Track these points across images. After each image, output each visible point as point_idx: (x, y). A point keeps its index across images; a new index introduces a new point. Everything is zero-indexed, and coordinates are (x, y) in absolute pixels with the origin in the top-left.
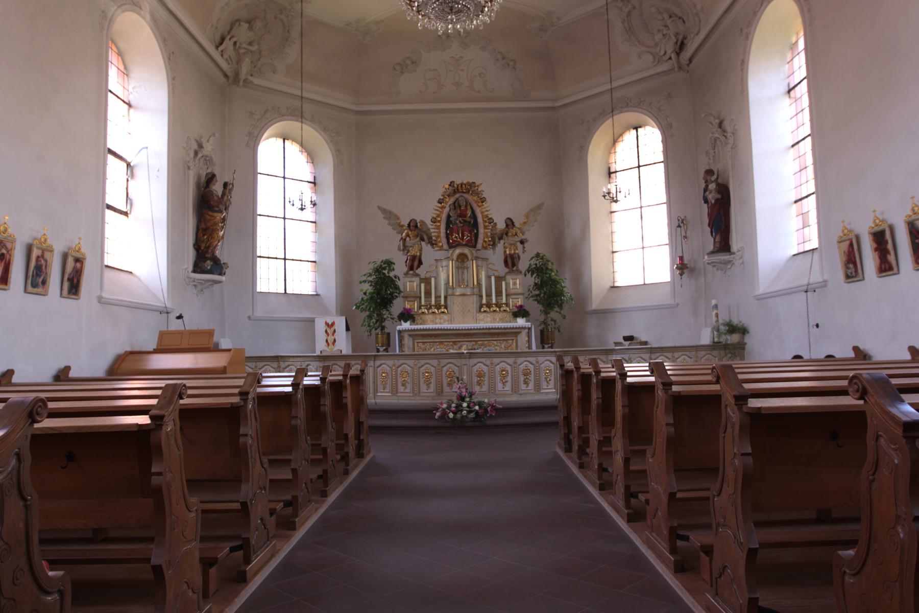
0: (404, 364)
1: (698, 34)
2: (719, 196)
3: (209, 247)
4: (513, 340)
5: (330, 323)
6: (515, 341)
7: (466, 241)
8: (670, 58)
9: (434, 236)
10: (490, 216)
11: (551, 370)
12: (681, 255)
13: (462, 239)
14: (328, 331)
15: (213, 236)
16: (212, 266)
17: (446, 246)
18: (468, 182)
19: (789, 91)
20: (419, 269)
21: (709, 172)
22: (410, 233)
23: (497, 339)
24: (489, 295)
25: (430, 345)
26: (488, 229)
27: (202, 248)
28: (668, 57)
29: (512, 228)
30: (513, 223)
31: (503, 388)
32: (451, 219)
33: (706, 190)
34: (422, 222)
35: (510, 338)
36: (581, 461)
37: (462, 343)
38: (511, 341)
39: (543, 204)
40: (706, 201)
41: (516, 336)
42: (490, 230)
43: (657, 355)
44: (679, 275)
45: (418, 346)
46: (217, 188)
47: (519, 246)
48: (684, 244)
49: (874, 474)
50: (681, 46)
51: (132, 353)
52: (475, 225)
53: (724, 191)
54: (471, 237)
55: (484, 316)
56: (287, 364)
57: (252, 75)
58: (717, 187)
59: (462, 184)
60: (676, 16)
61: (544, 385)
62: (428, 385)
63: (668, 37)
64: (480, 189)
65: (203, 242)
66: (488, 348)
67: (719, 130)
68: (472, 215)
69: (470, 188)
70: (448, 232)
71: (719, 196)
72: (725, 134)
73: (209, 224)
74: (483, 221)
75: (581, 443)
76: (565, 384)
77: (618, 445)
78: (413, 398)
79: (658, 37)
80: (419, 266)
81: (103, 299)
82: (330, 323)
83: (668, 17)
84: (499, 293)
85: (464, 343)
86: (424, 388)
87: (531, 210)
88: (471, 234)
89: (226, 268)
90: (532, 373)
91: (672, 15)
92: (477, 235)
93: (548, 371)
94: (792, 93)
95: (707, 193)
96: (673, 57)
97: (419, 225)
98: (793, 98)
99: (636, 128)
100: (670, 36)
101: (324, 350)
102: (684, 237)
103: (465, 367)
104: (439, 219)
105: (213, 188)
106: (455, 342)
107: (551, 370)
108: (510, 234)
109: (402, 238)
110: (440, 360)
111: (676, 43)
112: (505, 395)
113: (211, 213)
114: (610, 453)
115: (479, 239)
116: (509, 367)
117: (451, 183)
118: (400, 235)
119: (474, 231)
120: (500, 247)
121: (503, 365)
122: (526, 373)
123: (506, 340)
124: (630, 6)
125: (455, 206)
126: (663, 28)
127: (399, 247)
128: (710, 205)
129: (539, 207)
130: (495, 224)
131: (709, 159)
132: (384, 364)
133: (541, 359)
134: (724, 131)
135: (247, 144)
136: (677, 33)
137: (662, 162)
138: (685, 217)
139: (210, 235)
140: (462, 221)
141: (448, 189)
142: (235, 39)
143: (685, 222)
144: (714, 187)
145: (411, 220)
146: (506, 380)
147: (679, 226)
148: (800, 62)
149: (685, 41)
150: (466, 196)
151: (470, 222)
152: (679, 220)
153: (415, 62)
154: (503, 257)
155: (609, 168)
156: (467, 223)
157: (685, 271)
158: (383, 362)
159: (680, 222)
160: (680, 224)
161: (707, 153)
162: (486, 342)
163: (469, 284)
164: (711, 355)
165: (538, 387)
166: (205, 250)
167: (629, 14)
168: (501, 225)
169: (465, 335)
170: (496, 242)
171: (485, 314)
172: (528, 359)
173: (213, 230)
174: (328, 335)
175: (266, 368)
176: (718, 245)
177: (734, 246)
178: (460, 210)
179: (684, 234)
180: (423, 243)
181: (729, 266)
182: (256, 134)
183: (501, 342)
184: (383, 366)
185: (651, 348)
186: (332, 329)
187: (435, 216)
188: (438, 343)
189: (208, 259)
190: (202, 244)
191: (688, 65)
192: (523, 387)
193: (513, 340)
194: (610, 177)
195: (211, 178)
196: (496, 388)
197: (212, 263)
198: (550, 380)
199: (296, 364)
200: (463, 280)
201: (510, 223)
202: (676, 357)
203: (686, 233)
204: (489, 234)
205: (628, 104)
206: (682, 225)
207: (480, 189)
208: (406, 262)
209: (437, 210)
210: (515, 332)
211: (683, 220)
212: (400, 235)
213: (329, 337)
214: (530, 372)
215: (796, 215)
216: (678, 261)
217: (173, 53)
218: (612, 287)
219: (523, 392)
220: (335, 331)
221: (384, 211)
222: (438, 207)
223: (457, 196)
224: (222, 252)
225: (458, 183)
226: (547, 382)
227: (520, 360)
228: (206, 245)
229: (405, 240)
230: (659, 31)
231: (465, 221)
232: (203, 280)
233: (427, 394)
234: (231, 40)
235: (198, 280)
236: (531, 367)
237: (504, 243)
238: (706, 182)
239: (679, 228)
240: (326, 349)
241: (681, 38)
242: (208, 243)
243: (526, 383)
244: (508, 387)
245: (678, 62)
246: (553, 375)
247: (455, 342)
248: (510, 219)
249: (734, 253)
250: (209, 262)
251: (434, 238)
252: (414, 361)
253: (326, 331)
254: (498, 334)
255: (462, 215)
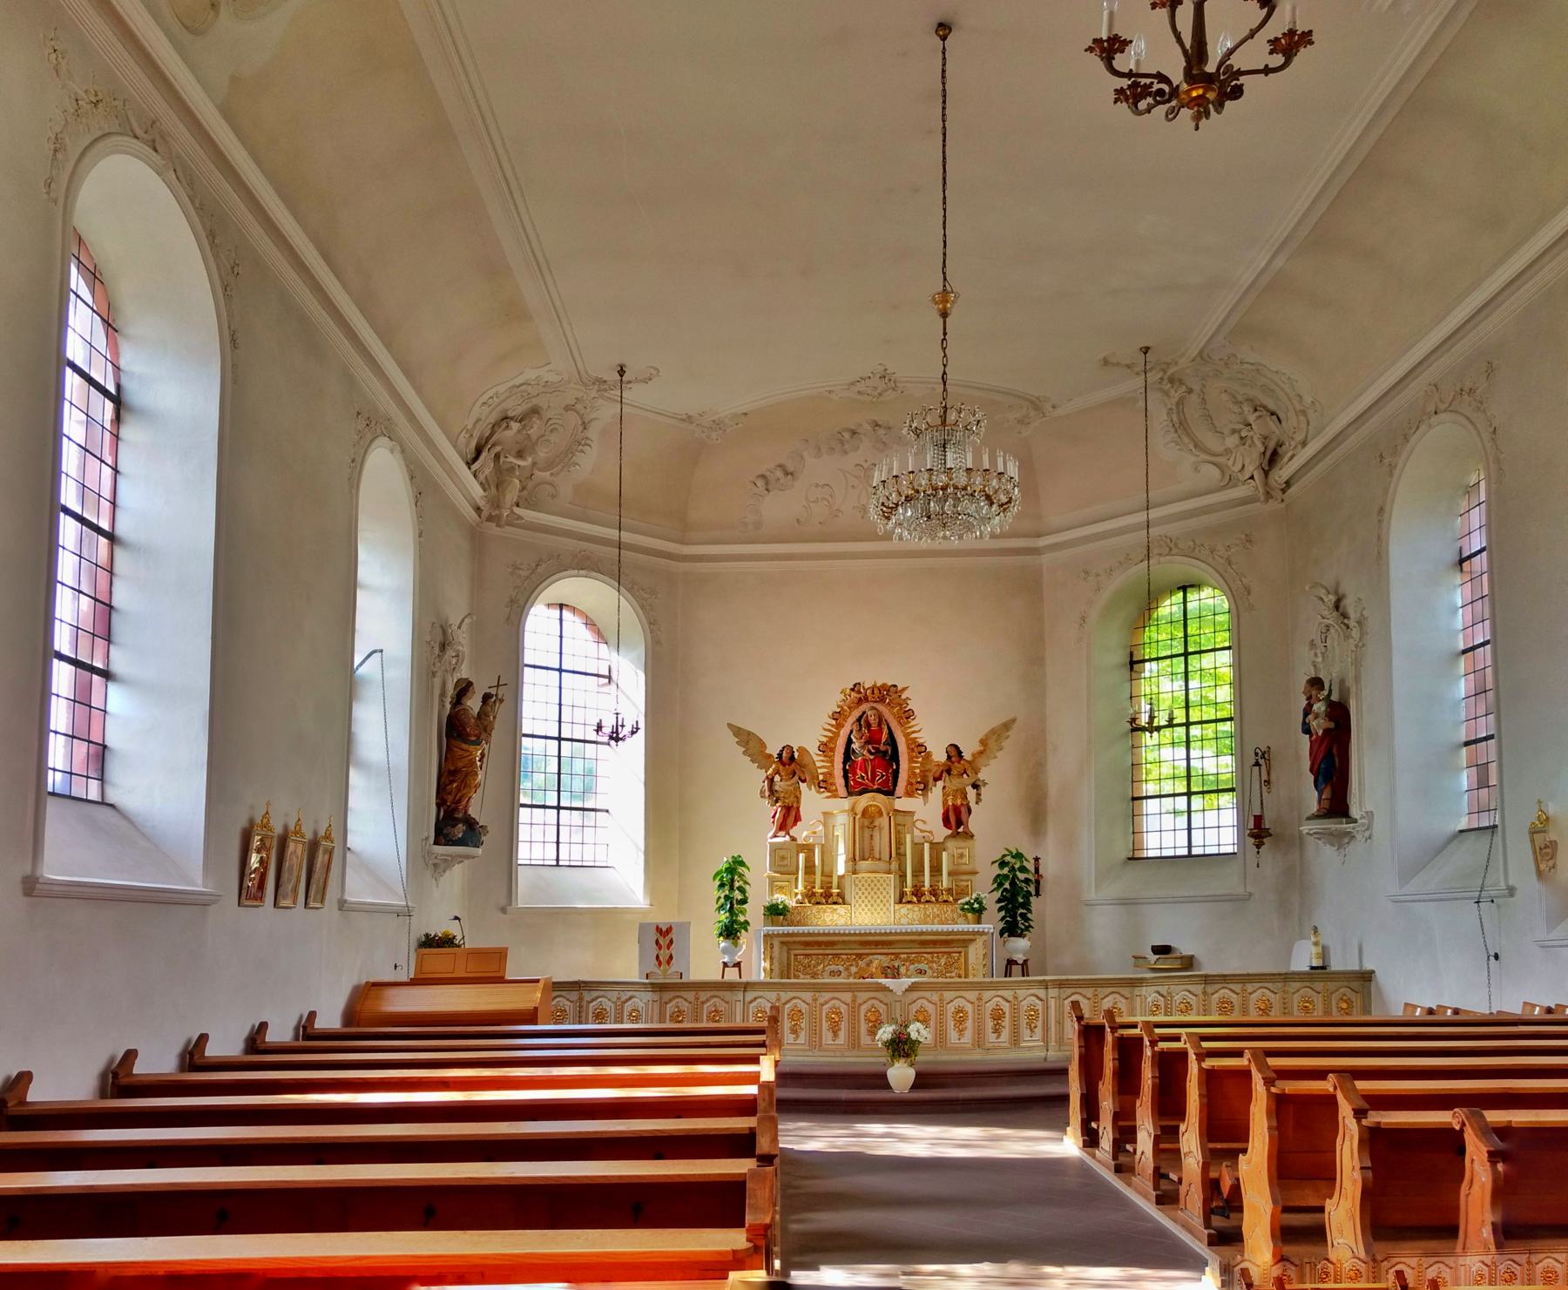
0: (794, 998)
1: (1304, 444)
2: (1331, 725)
3: (459, 801)
4: (960, 953)
5: (664, 929)
6: (963, 954)
7: (879, 785)
8: (1252, 477)
9: (821, 774)
10: (920, 741)
11: (1038, 1010)
12: (1258, 814)
13: (873, 781)
14: (661, 942)
15: (468, 782)
16: (464, 832)
17: (842, 791)
18: (884, 685)
19: (1462, 561)
20: (795, 828)
21: (1316, 683)
22: (781, 767)
23: (932, 950)
24: (918, 872)
25: (818, 958)
26: (917, 762)
27: (449, 804)
28: (1248, 475)
29: (959, 762)
30: (959, 753)
31: (959, 1039)
32: (853, 746)
33: (1307, 711)
34: (802, 750)
35: (956, 949)
36: (1118, 1162)
37: (871, 957)
38: (957, 955)
39: (1013, 721)
40: (1307, 730)
41: (967, 947)
42: (919, 765)
43: (1218, 986)
44: (1254, 847)
45: (796, 960)
46: (473, 704)
47: (971, 793)
48: (1265, 794)
49: (1469, 1189)
50: (1273, 458)
51: (375, 985)
52: (895, 756)
53: (1339, 714)
54: (888, 777)
55: (908, 909)
56: (595, 994)
57: (518, 506)
58: (1329, 710)
59: (873, 689)
60: (1265, 407)
61: (1026, 1033)
62: (835, 1034)
63: (1249, 442)
64: (903, 697)
65: (450, 794)
66: (916, 965)
67: (1335, 613)
68: (889, 740)
69: (886, 694)
70: (847, 767)
71: (1331, 725)
72: (1346, 621)
73: (460, 764)
74: (908, 748)
75: (1118, 1136)
76: (1083, 1044)
77: (1190, 1140)
78: (810, 1053)
79: (1232, 441)
80: (795, 823)
81: (345, 905)
82: (664, 929)
83: (1252, 410)
84: (936, 870)
85: (875, 956)
86: (827, 1037)
87: (993, 732)
88: (887, 772)
89: (485, 835)
90: (1007, 1015)
91: (1258, 408)
92: (896, 774)
93: (1033, 1013)
94: (1466, 565)
95: (1310, 717)
96: (1255, 477)
97: (796, 755)
98: (1467, 572)
99: (1184, 589)
100: (1253, 441)
101: (652, 973)
102: (1265, 781)
103: (898, 1004)
104: (832, 746)
105: (468, 704)
106: (860, 956)
107: (1038, 1010)
108: (954, 772)
109: (767, 777)
110: (856, 993)
111: (1264, 453)
112: (962, 1050)
113: (465, 746)
114: (1177, 1152)
115: (900, 780)
116: (970, 1005)
117: (855, 685)
118: (764, 770)
119: (892, 766)
120: (936, 792)
121: (960, 1002)
122: (998, 1016)
123: (949, 953)
124: (1184, 388)
125: (860, 725)
126: (1241, 426)
127: (762, 792)
128: (1314, 737)
129: (1007, 726)
130: (929, 755)
131: (1316, 655)
132: (760, 997)
133: (1021, 993)
134: (1345, 616)
135: (508, 620)
136: (1266, 438)
137: (1229, 648)
138: (1269, 748)
139: (463, 781)
140: (873, 751)
141: (850, 696)
142: (498, 449)
143: (1266, 756)
144: (1323, 708)
145: (784, 748)
146: (964, 1026)
147: (1257, 764)
148: (1476, 517)
149: (1280, 451)
150: (880, 707)
151: (886, 751)
152: (1256, 754)
153: (792, 474)
154: (941, 811)
155: (1131, 655)
156: (881, 754)
157: (1265, 840)
158: (761, 993)
159: (1259, 758)
160: (1260, 760)
161: (1312, 644)
162: (914, 955)
163: (882, 857)
164: (1311, 988)
165: (1016, 1039)
166: (453, 806)
167: (1180, 403)
168: (940, 756)
169: (877, 944)
170: (930, 786)
171: (909, 906)
172: (1000, 993)
173: (467, 775)
174: (660, 948)
175: (558, 1002)
176: (1326, 804)
177: (1355, 811)
178: (869, 731)
179: (1265, 777)
180: (803, 786)
181: (1346, 840)
182: (521, 602)
183: (940, 955)
184: (760, 1000)
185: (1206, 976)
186: (668, 938)
187: (825, 740)
188: (830, 957)
189: (457, 821)
190: (449, 796)
191: (1284, 491)
192: (992, 1037)
193: (960, 953)
194: (1132, 669)
195: (464, 689)
196: (948, 1038)
197: (465, 828)
198: (1035, 1027)
199: (609, 994)
200: (872, 849)
201: (953, 753)
202: (1249, 991)
203: (1269, 774)
204: (918, 771)
205: (1171, 549)
206: (1262, 762)
207: (903, 697)
208: (774, 817)
209: (829, 731)
210: (964, 941)
211: (1263, 754)
212: (764, 770)
213: (662, 952)
214: (1004, 1013)
215: (1465, 766)
216: (1251, 825)
217: (420, 494)
218: (1129, 859)
219: (991, 1045)
220: (671, 942)
221: (737, 731)
222: (829, 724)
223: (864, 707)
224: (478, 807)
225: (866, 687)
226: (1031, 1030)
227: (987, 995)
228: (455, 797)
229: (773, 779)
230: (1234, 431)
231: (877, 750)
232: (451, 856)
233: (834, 1047)
234: (491, 451)
235: (442, 855)
236: (1006, 1007)
237: (944, 788)
238: (1309, 698)
239: (1258, 767)
240: (656, 970)
241: (1272, 445)
242: (460, 794)
243: (997, 1031)
244: (968, 1038)
245: (1266, 484)
246: (1040, 1019)
247: (860, 956)
248: (956, 747)
249: (1355, 821)
250: (460, 825)
251: (821, 777)
252: (812, 994)
253: (657, 942)
254: (935, 943)
255: (872, 739)
